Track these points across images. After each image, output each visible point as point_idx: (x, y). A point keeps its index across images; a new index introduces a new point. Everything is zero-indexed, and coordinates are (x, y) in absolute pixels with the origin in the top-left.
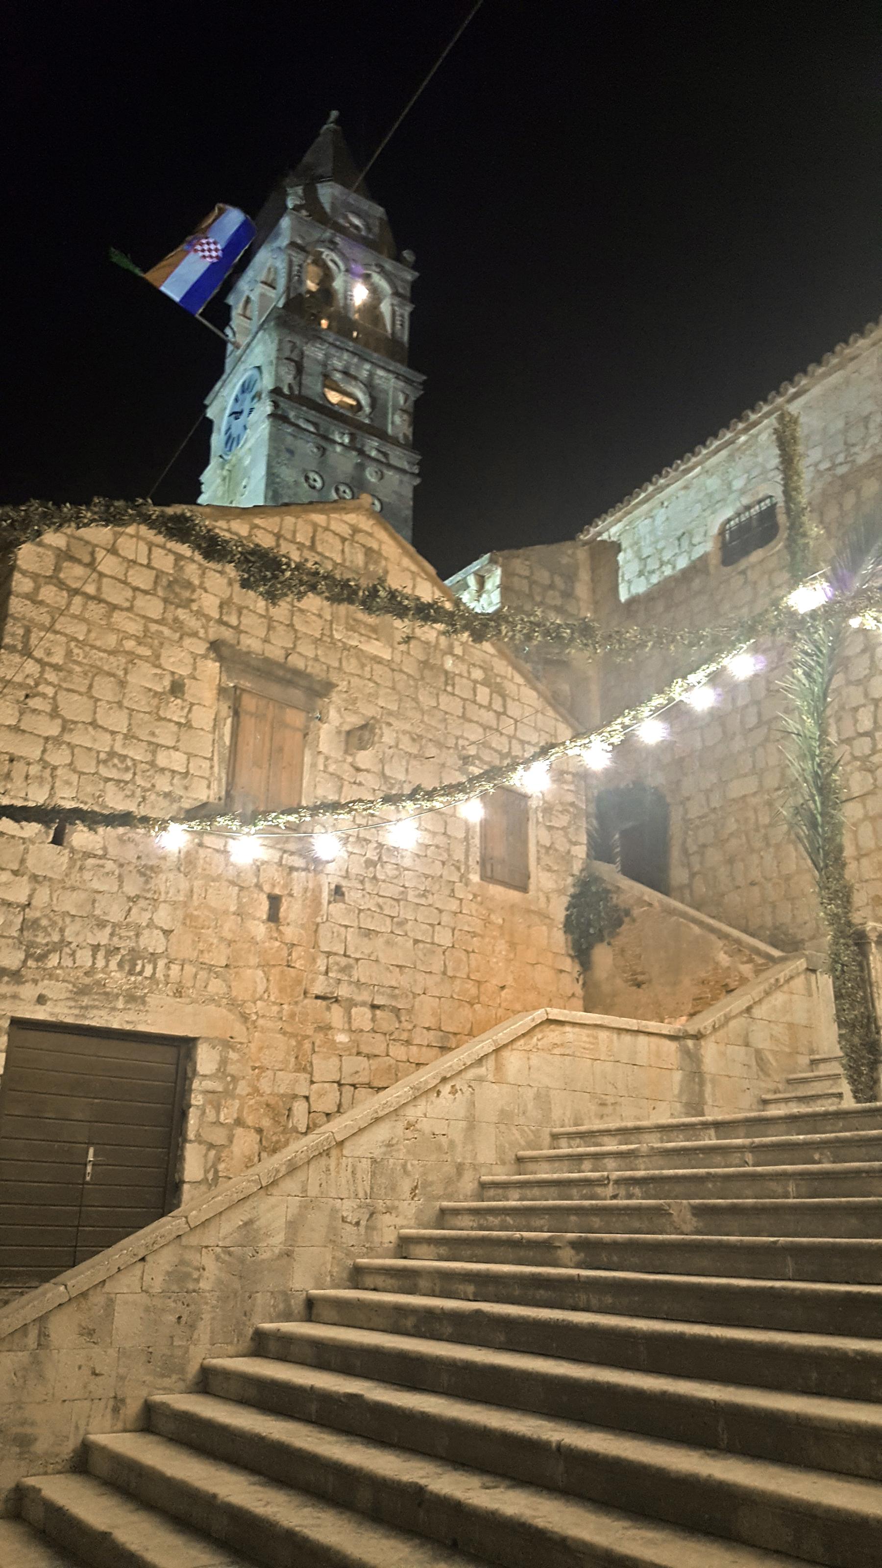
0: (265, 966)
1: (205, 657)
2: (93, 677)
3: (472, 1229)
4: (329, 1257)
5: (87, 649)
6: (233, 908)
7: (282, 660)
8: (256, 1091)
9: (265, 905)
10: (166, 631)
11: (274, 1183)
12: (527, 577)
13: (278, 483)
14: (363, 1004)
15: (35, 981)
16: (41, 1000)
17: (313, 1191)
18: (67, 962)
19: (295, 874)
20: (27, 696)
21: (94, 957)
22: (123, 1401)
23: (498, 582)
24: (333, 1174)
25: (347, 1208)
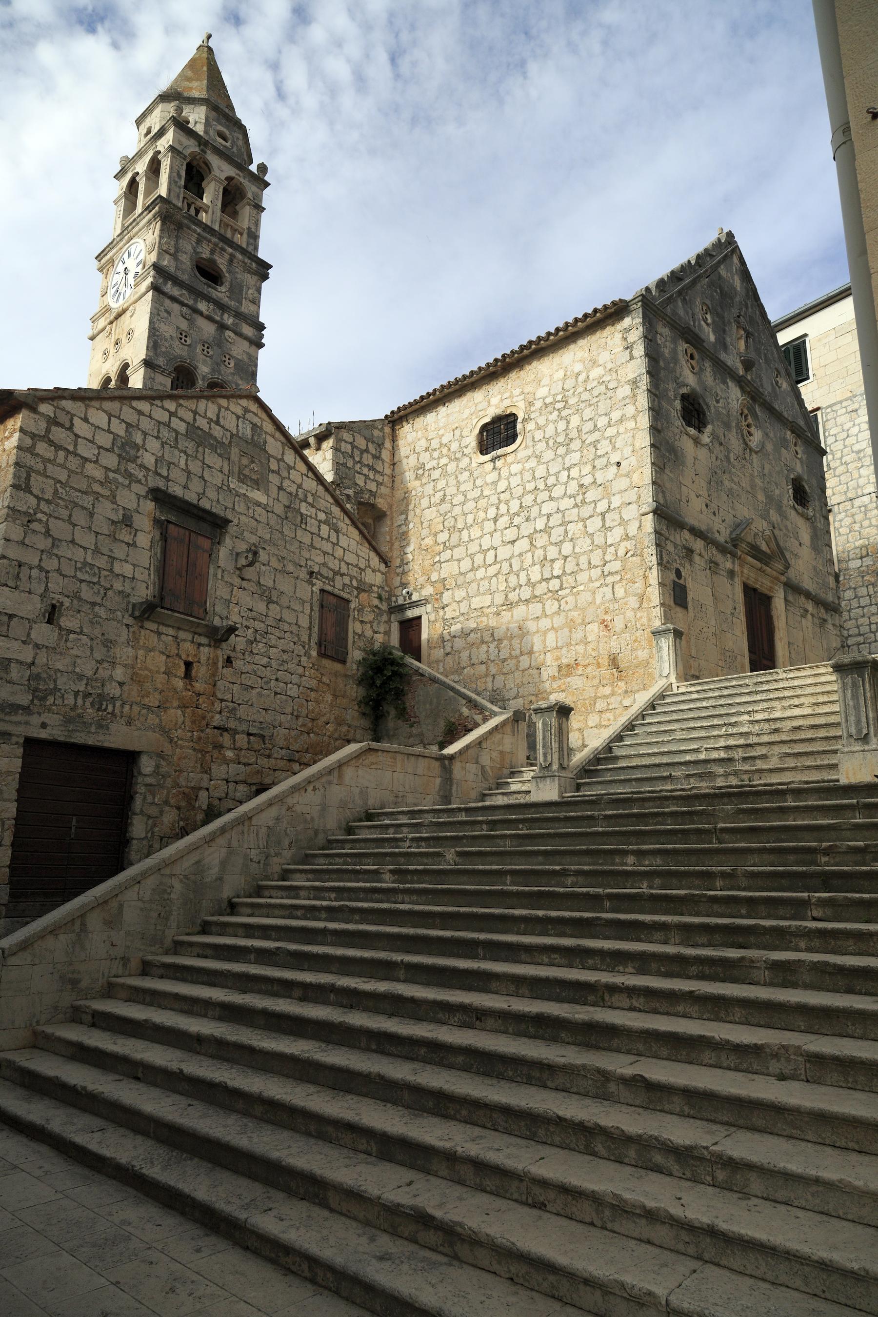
0: (183, 707)
1: (145, 497)
2: (72, 509)
3: (325, 864)
4: (243, 881)
5: (68, 489)
6: (163, 670)
7: (195, 502)
8: (178, 785)
9: (183, 668)
10: (121, 479)
11: (212, 840)
12: (351, 443)
13: (158, 336)
14: (243, 732)
15: (39, 714)
16: (44, 725)
17: (235, 844)
18: (59, 701)
19: (202, 648)
20: (29, 521)
21: (76, 700)
22: (128, 960)
23: (331, 445)
24: (246, 835)
25: (253, 854)
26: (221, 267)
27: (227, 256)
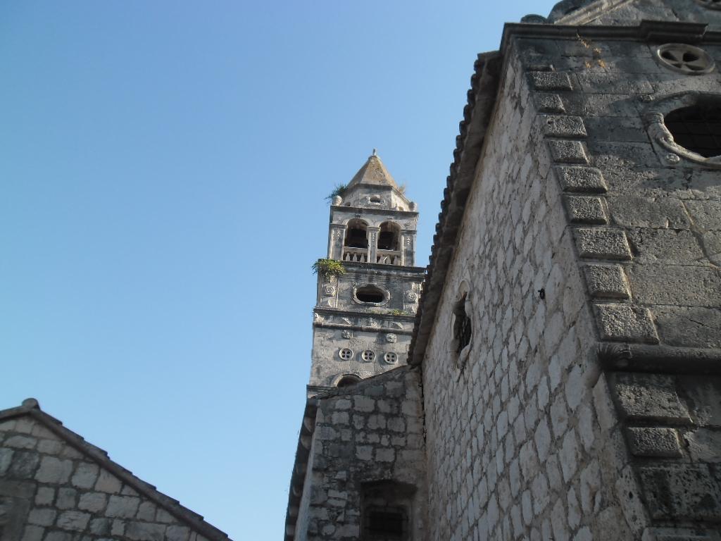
12: (348, 410)
26: (379, 287)
27: (385, 278)
